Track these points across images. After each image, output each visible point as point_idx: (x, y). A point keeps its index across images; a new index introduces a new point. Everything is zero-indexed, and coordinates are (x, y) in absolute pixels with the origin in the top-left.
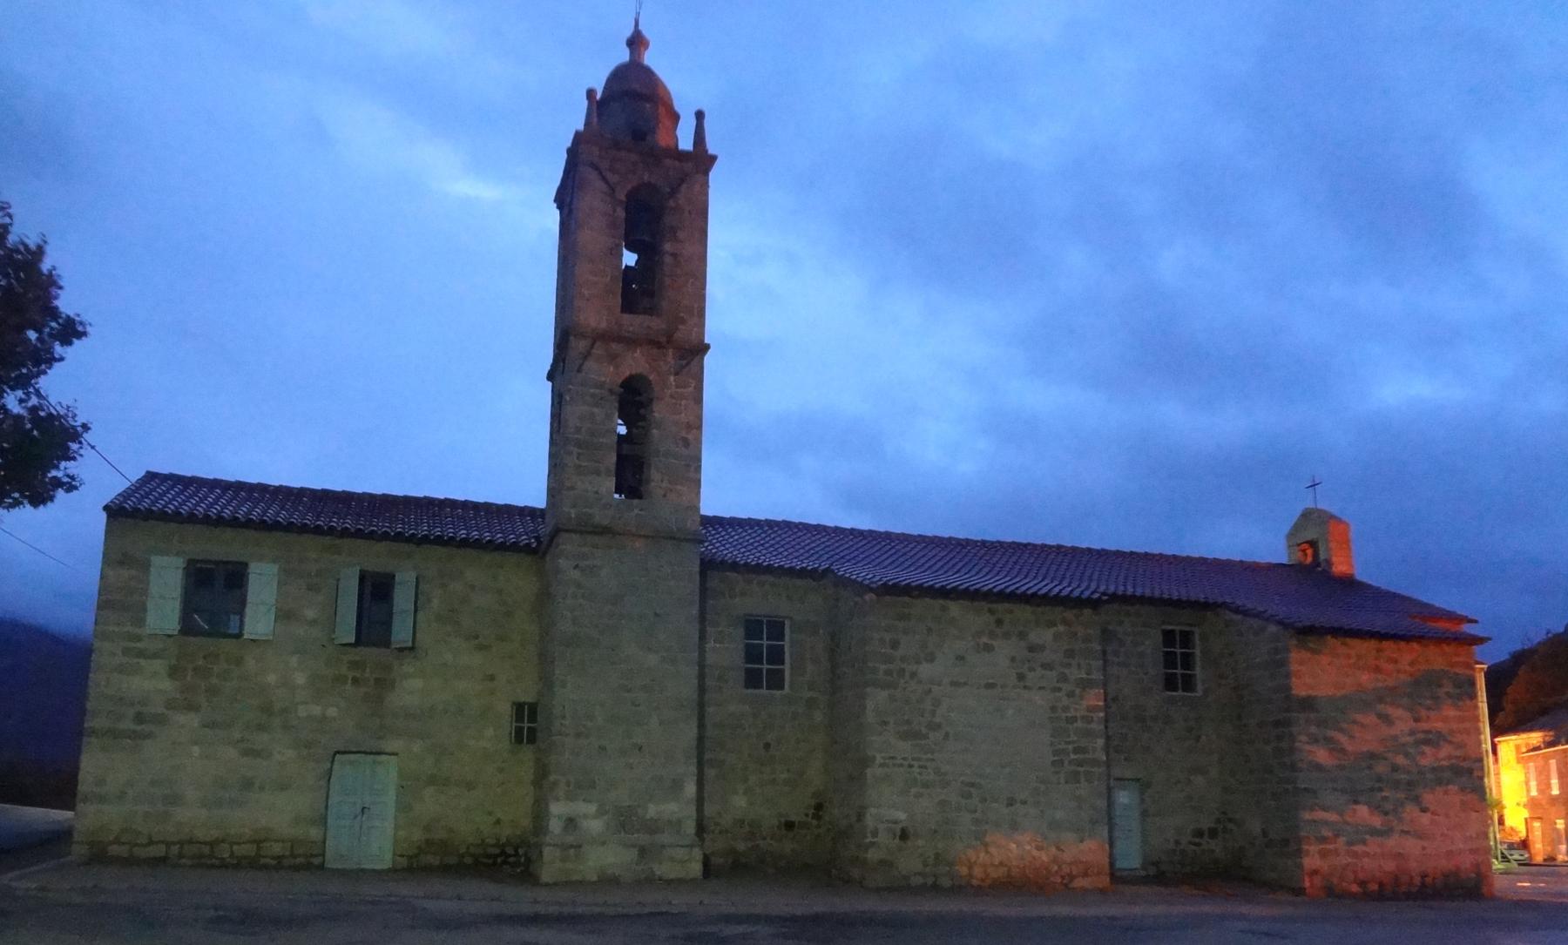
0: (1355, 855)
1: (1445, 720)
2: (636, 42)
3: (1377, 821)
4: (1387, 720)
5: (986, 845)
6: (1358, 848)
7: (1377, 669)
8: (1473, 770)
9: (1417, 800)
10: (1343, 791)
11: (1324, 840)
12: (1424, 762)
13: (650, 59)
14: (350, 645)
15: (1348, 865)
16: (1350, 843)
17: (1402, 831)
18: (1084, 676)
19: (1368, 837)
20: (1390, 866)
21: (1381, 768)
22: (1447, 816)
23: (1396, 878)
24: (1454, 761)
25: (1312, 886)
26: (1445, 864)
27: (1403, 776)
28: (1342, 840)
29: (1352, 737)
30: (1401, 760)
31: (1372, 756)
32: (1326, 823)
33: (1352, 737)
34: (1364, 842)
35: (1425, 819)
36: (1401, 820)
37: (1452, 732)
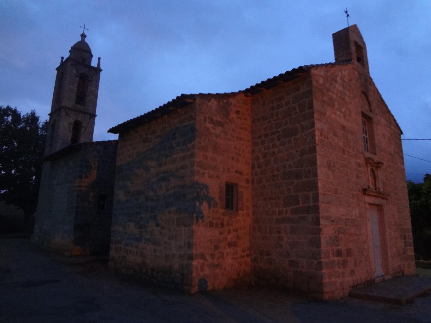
2: (83, 36)
13: (87, 40)
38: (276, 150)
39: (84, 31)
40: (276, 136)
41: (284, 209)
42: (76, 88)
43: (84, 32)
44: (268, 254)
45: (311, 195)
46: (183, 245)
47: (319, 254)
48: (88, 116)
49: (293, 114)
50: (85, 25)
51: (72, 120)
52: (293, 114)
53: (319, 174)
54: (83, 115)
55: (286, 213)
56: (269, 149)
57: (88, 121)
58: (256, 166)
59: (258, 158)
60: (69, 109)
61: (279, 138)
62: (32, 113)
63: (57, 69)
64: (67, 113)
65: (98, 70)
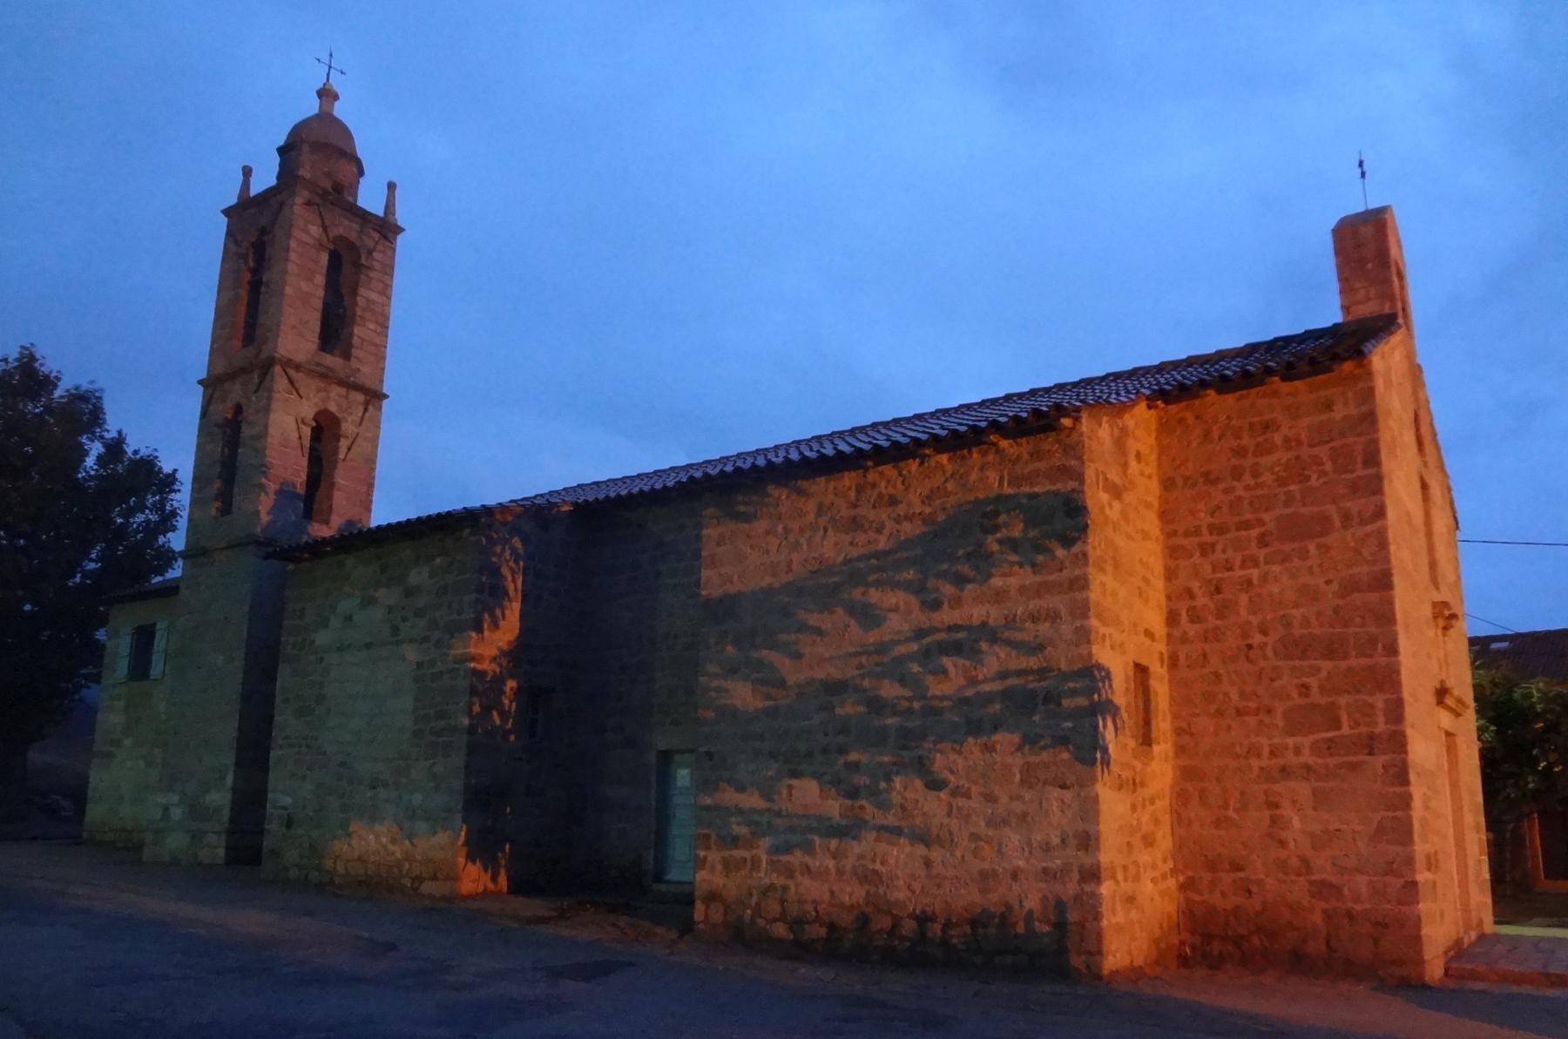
0: (789, 872)
1: (1000, 596)
2: (327, 95)
3: (834, 807)
4: (868, 616)
5: (349, 835)
6: (797, 858)
7: (855, 524)
8: (1238, 716)
9: (921, 767)
10: (773, 755)
11: (735, 841)
12: (936, 688)
13: (340, 110)
14: (682, 752)
15: (772, 887)
16: (776, 850)
17: (882, 828)
18: (455, 616)
19: (817, 840)
20: (853, 893)
21: (848, 708)
22: (990, 798)
23: (864, 921)
24: (1013, 681)
25: (706, 920)
26: (968, 897)
27: (890, 721)
28: (766, 842)
29: (798, 656)
30: (890, 690)
31: (836, 688)
32: (740, 811)
33: (798, 656)
34: (809, 848)
35: (933, 806)
36: (884, 806)
37: (1011, 622)
38: (1255, 573)
39: (328, 75)
40: (1255, 533)
41: (1290, 741)
42: (321, 293)
43: (328, 79)
44: (1236, 867)
45: (1380, 705)
46: (1056, 841)
47: (1410, 861)
48: (360, 397)
49: (1314, 476)
50: (331, 55)
51: (308, 411)
52: (1314, 476)
53: (1401, 649)
54: (343, 391)
55: (1298, 751)
56: (1231, 569)
57: (360, 414)
58: (1184, 617)
59: (1190, 594)
60: (298, 367)
61: (1262, 541)
62: (22, 356)
63: (227, 212)
64: (291, 382)
65: (387, 228)
